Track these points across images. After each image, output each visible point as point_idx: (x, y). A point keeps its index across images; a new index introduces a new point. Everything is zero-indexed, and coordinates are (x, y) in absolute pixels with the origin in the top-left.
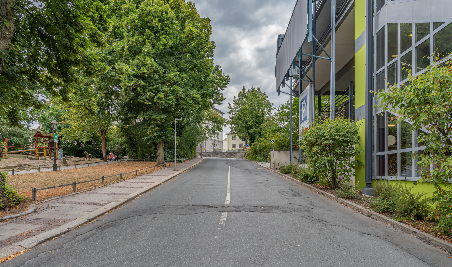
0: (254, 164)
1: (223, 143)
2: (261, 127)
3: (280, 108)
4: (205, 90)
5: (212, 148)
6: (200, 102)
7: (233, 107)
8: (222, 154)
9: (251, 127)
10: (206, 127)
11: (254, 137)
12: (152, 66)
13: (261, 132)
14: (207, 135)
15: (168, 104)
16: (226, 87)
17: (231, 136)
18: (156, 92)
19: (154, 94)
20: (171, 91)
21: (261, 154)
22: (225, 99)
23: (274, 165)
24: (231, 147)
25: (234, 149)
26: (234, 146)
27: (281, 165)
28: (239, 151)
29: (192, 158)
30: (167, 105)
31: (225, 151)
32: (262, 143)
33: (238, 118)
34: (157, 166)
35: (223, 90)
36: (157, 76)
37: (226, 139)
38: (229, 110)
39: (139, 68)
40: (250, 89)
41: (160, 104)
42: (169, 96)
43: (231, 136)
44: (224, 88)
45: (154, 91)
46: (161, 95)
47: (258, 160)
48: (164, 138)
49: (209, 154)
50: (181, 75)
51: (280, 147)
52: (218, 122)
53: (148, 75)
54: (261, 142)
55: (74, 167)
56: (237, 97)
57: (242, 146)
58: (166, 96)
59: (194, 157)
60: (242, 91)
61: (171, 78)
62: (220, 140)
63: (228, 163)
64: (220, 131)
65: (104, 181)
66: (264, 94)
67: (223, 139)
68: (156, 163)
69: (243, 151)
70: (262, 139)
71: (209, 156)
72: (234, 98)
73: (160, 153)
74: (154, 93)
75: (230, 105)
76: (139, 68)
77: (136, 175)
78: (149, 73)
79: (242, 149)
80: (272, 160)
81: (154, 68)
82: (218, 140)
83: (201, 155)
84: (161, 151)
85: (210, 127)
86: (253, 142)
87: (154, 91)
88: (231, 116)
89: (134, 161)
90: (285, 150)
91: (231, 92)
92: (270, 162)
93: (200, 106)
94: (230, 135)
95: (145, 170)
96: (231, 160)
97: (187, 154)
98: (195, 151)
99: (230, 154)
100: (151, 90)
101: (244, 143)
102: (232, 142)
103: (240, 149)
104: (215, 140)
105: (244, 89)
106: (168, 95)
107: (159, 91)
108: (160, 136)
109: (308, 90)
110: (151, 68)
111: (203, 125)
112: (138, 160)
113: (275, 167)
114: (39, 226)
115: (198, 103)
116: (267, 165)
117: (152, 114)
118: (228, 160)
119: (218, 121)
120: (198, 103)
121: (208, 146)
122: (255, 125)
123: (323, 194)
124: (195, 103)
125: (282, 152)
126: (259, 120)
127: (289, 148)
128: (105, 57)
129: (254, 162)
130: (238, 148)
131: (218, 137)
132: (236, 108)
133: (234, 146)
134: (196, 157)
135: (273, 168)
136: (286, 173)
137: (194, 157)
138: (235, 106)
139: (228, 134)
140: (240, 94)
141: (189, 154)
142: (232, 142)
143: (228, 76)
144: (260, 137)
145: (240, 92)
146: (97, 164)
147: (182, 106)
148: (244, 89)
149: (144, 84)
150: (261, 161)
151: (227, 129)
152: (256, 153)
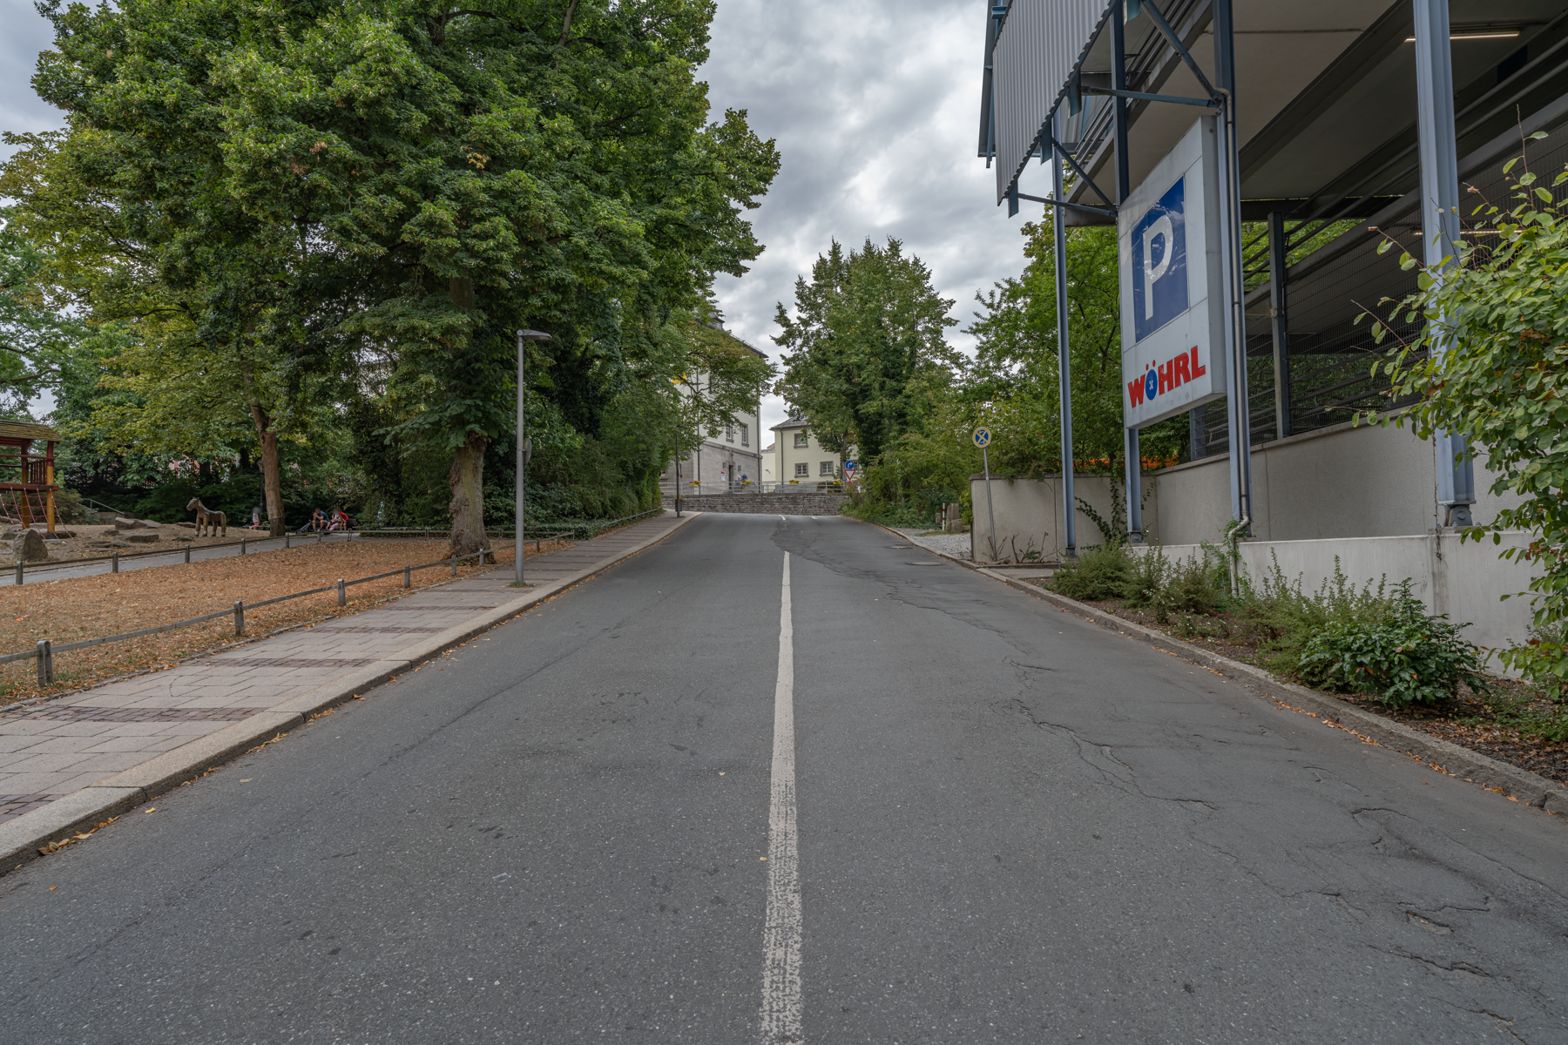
0: (888, 538)
1: (763, 461)
2: (907, 391)
3: (998, 292)
4: (668, 206)
5: (724, 478)
6: (647, 258)
7: (794, 321)
8: (761, 501)
9: (865, 393)
10: (696, 397)
11: (879, 431)
12: (385, 60)
13: (908, 410)
14: (702, 431)
15: (474, 254)
16: (763, 192)
17: (789, 437)
18: (417, 196)
19: (400, 205)
20: (502, 194)
21: (928, 495)
22: (762, 249)
23: (993, 547)
24: (790, 475)
25: (802, 481)
26: (802, 469)
27: (1022, 546)
28: (821, 486)
29: (641, 518)
30: (473, 262)
31: (772, 488)
32: (911, 454)
33: (818, 361)
34: (446, 561)
35: (750, 205)
36: (416, 114)
37: (771, 449)
38: (780, 331)
39: (325, 75)
40: (860, 251)
41: (438, 256)
42: (481, 219)
43: (789, 437)
44: (754, 199)
45: (402, 190)
46: (442, 211)
47: (901, 522)
48: (477, 428)
49: (709, 502)
50: (543, 120)
51: (1011, 463)
52: (739, 371)
53: (372, 104)
54: (907, 451)
55: (107, 567)
56: (810, 282)
57: (831, 469)
58: (465, 217)
59: (651, 515)
60: (828, 258)
61: (492, 132)
62: (752, 449)
63: (785, 536)
64: (749, 411)
65: (242, 627)
66: (916, 262)
67: (764, 446)
68: (444, 546)
69: (836, 488)
70: (913, 437)
71: (713, 508)
72: (801, 284)
73: (465, 502)
74: (401, 198)
75: (783, 312)
76: (325, 75)
77: (239, 634)
78: (371, 93)
79: (831, 479)
80: (981, 524)
81: (395, 68)
82: (744, 449)
83: (679, 504)
84: (469, 491)
85: (707, 397)
86: (877, 452)
87: (402, 190)
88: (789, 353)
89: (389, 535)
90: (1038, 476)
91: (789, 252)
92: (967, 526)
93: (645, 274)
94: (786, 433)
95: (334, 594)
96: (792, 524)
97: (616, 503)
98: (654, 492)
99: (789, 499)
100: (389, 189)
101: (835, 458)
102: (795, 456)
103: (824, 479)
104: (733, 452)
105: (835, 251)
106: (476, 212)
107: (430, 192)
108: (459, 422)
109: (1193, 162)
110: (382, 67)
111: (685, 391)
112: (404, 530)
113: (995, 558)
114: (1402, 221)
115: (636, 260)
116: (952, 544)
117: (399, 310)
118: (779, 524)
119: (740, 372)
120: (636, 260)
121: (706, 471)
122: (882, 387)
123: (1412, 748)
124: (622, 263)
125: (1024, 484)
126: (897, 364)
127: (1054, 468)
128: (174, 41)
129: (882, 530)
130: (814, 476)
131: (745, 437)
132: (805, 323)
133: (802, 469)
134: (661, 511)
135: (986, 559)
136: (1090, 598)
137: (648, 511)
138: (804, 316)
139: (779, 429)
140: (821, 270)
141: (629, 501)
142: (795, 456)
143: (771, 144)
144: (902, 432)
145: (823, 261)
146: (235, 551)
147: (555, 273)
148: (835, 251)
149: (346, 150)
150: (910, 524)
151: (773, 408)
152: (887, 493)
